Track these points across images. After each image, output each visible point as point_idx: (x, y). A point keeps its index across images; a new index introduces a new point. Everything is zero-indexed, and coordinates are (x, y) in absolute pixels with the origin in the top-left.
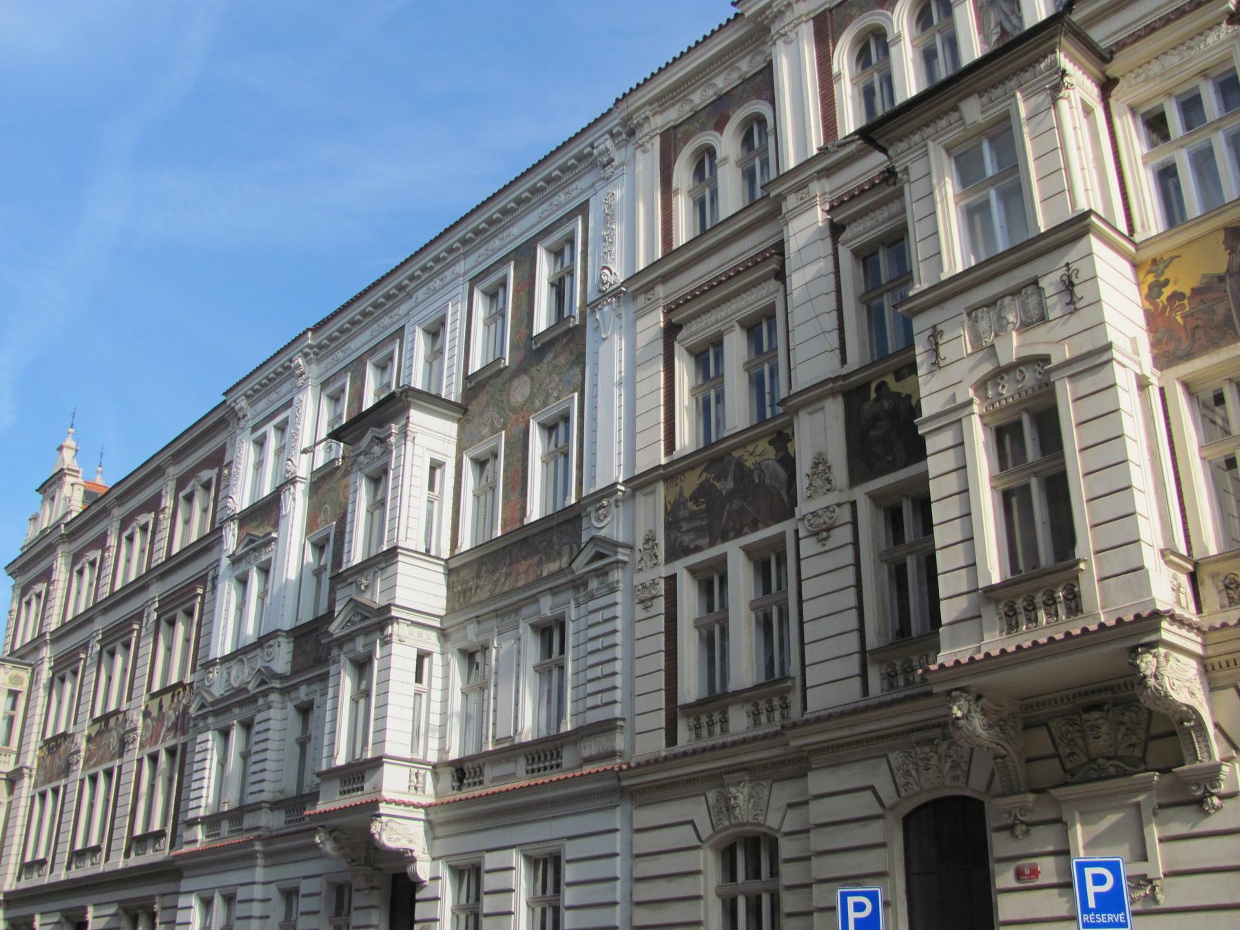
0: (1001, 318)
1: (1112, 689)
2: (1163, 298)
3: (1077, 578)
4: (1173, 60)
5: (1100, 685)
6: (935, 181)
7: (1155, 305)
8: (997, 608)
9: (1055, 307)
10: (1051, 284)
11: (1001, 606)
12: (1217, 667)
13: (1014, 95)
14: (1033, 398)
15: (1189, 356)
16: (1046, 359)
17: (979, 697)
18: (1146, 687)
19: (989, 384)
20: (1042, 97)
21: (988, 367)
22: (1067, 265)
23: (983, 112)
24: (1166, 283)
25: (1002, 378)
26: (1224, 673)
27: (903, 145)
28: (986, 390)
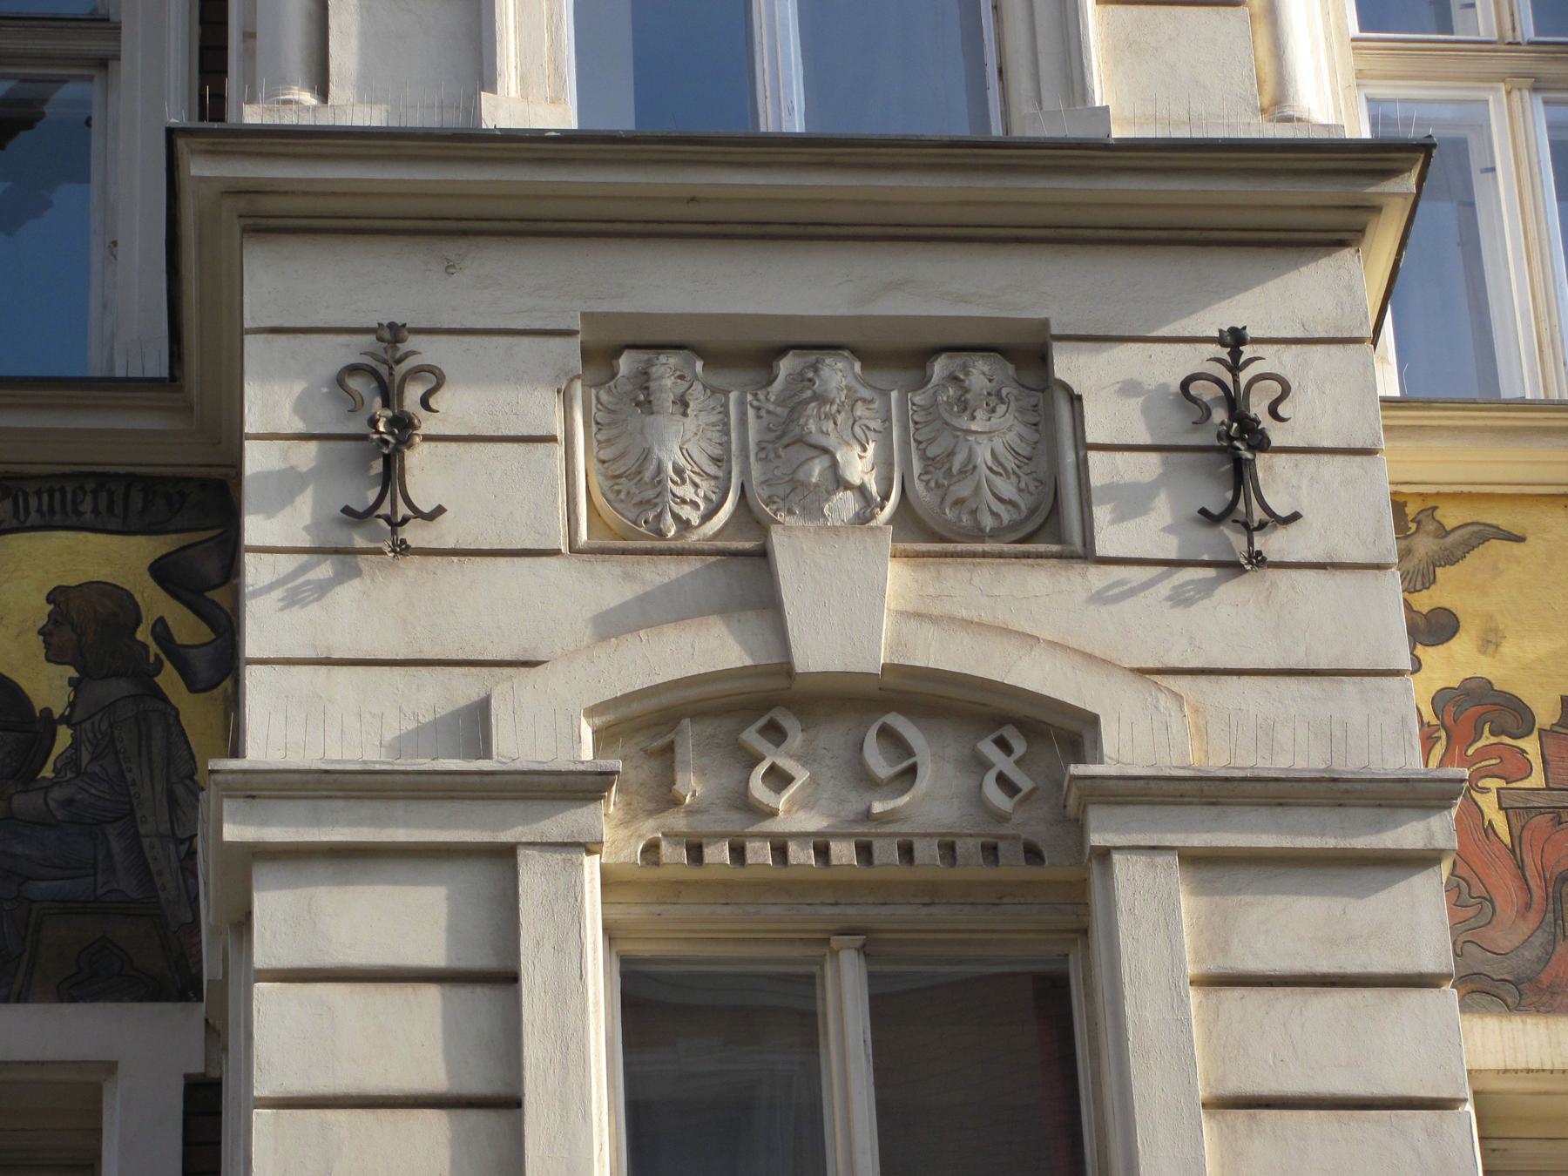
9: (1137, 509)
14: (931, 892)
16: (1070, 732)
21: (713, 649)
22: (1235, 339)
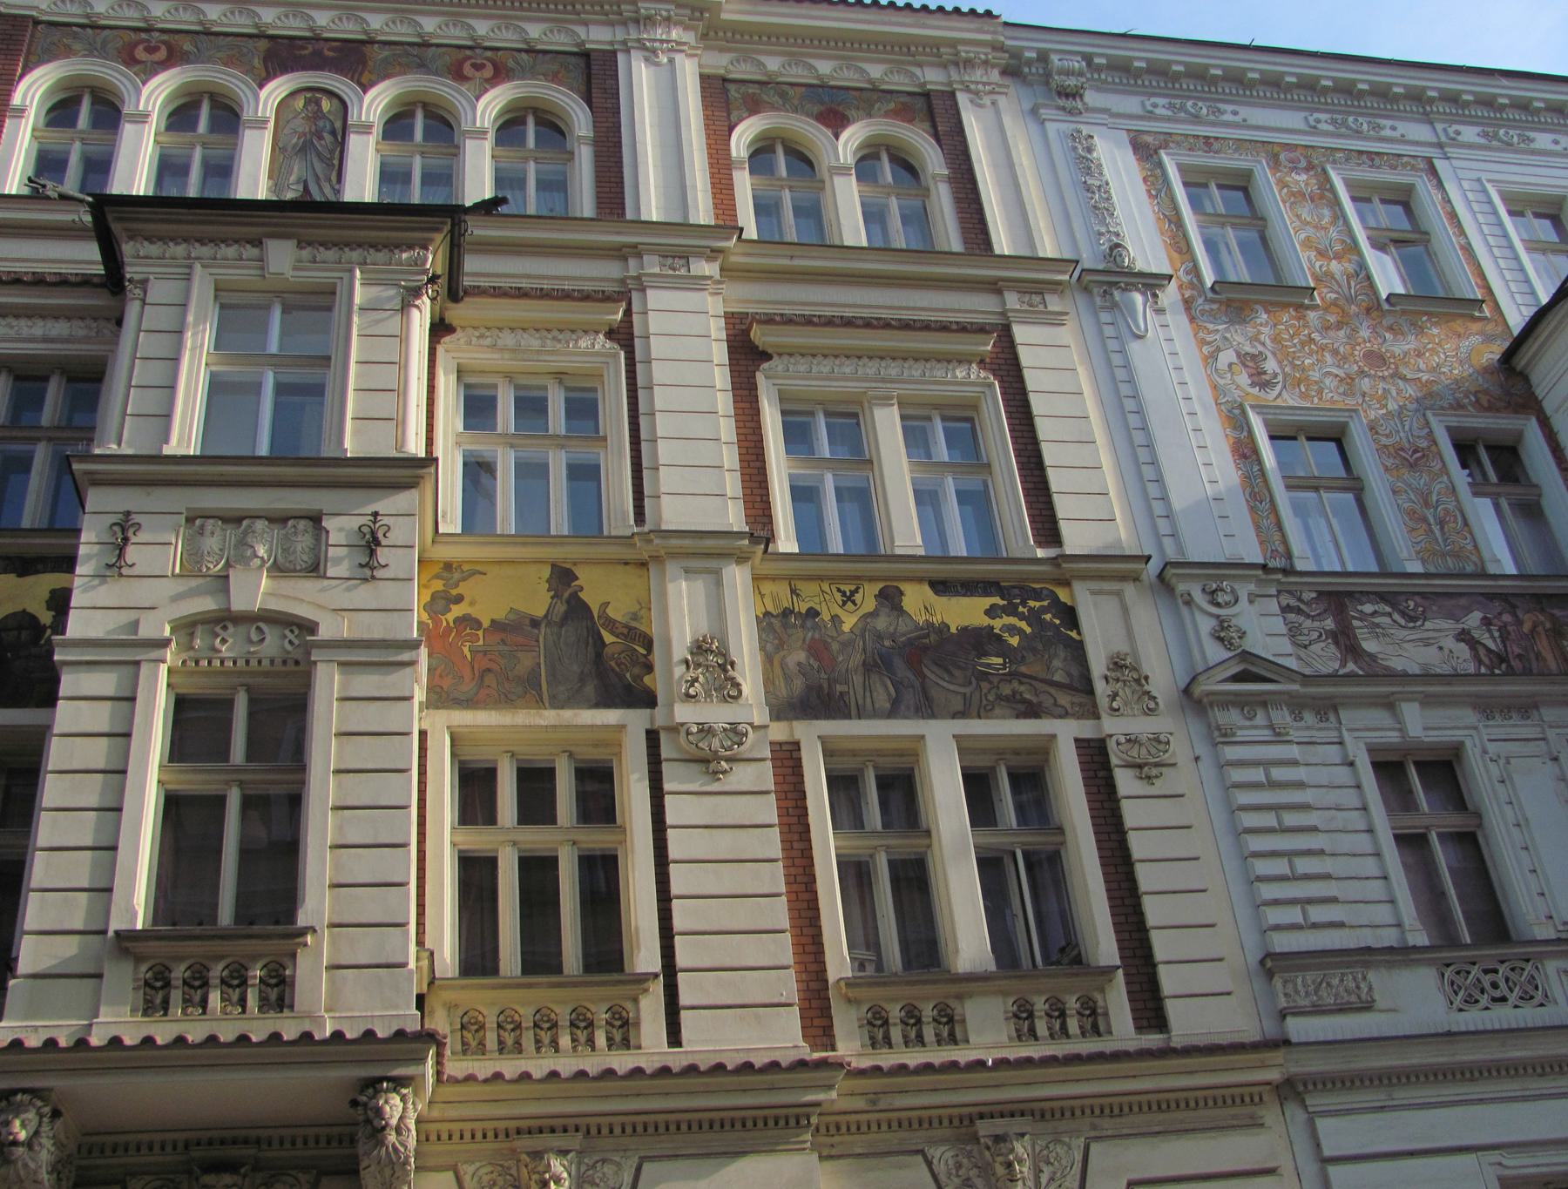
0: (243, 543)
1: (258, 1141)
2: (451, 617)
3: (294, 956)
4: (533, 342)
5: (243, 1133)
6: (190, 319)
7: (437, 623)
8: (136, 968)
9: (340, 563)
10: (341, 530)
11: (144, 968)
12: (433, 1137)
13: (351, 271)
14: (267, 674)
15: (468, 703)
16: (310, 627)
17: (56, 1114)
18: (381, 1143)
19: (199, 630)
20: (392, 292)
22: (376, 514)
23: (295, 269)
24: (459, 599)
25: (225, 628)
26: (439, 1148)
27: (154, 249)
28: (192, 635)
